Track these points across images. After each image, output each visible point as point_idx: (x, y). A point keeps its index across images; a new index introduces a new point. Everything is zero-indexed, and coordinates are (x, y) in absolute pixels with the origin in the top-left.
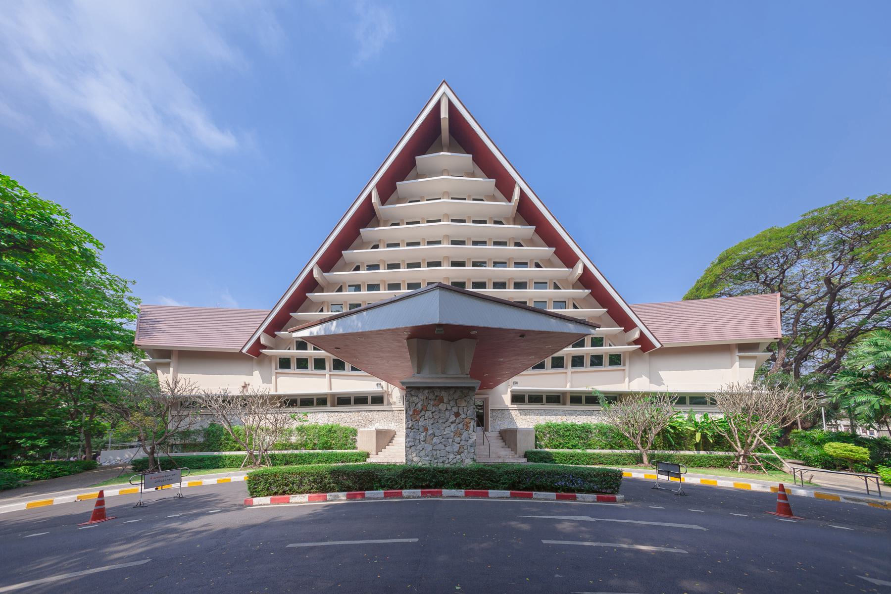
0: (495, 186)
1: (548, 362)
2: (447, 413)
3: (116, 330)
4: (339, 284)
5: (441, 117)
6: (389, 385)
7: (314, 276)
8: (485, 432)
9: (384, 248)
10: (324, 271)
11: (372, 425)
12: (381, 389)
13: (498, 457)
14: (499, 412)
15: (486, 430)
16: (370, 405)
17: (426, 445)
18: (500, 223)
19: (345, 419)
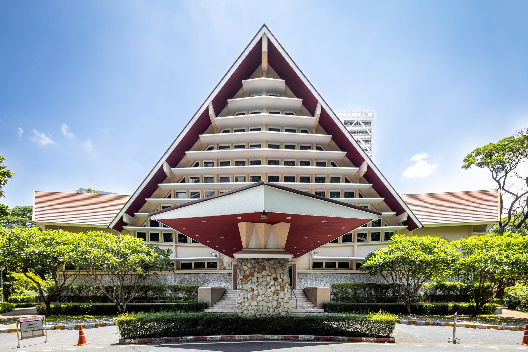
0: (302, 103)
1: (340, 239)
2: (268, 278)
4: (182, 177)
5: (262, 51)
6: (221, 254)
7: (164, 171)
8: (293, 290)
9: (218, 150)
10: (172, 167)
11: (208, 284)
12: (215, 257)
13: (303, 309)
14: (303, 275)
15: (294, 288)
16: (206, 269)
17: (252, 301)
18: (306, 132)
19: (188, 279)
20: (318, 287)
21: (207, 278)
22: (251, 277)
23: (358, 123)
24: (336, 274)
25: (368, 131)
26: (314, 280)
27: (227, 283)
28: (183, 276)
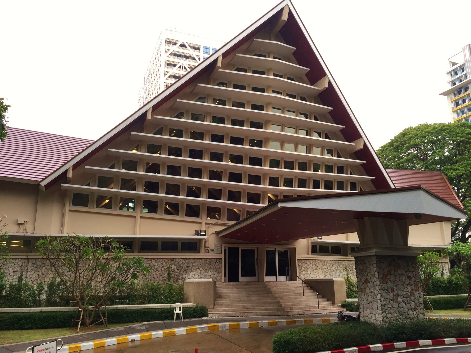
3: (445, 255)
19: (156, 267)
20: (335, 279)
21: (186, 264)
22: (390, 276)
23: (182, 46)
24: (334, 261)
25: (196, 58)
26: (314, 269)
27: (215, 273)
28: (149, 262)
